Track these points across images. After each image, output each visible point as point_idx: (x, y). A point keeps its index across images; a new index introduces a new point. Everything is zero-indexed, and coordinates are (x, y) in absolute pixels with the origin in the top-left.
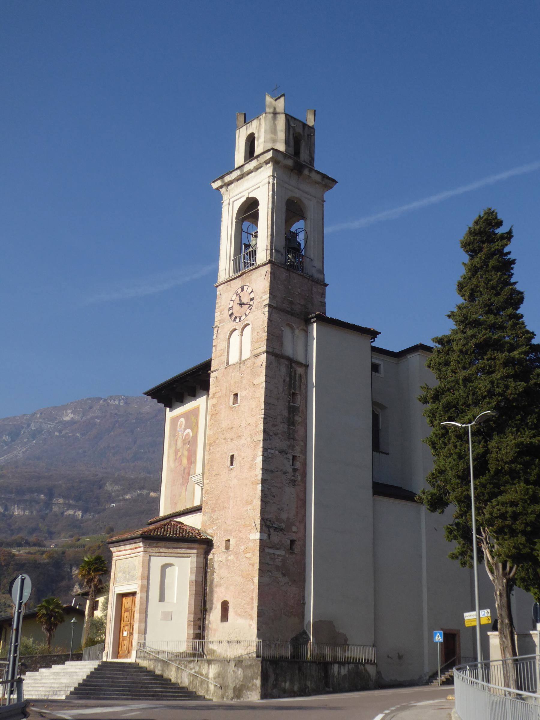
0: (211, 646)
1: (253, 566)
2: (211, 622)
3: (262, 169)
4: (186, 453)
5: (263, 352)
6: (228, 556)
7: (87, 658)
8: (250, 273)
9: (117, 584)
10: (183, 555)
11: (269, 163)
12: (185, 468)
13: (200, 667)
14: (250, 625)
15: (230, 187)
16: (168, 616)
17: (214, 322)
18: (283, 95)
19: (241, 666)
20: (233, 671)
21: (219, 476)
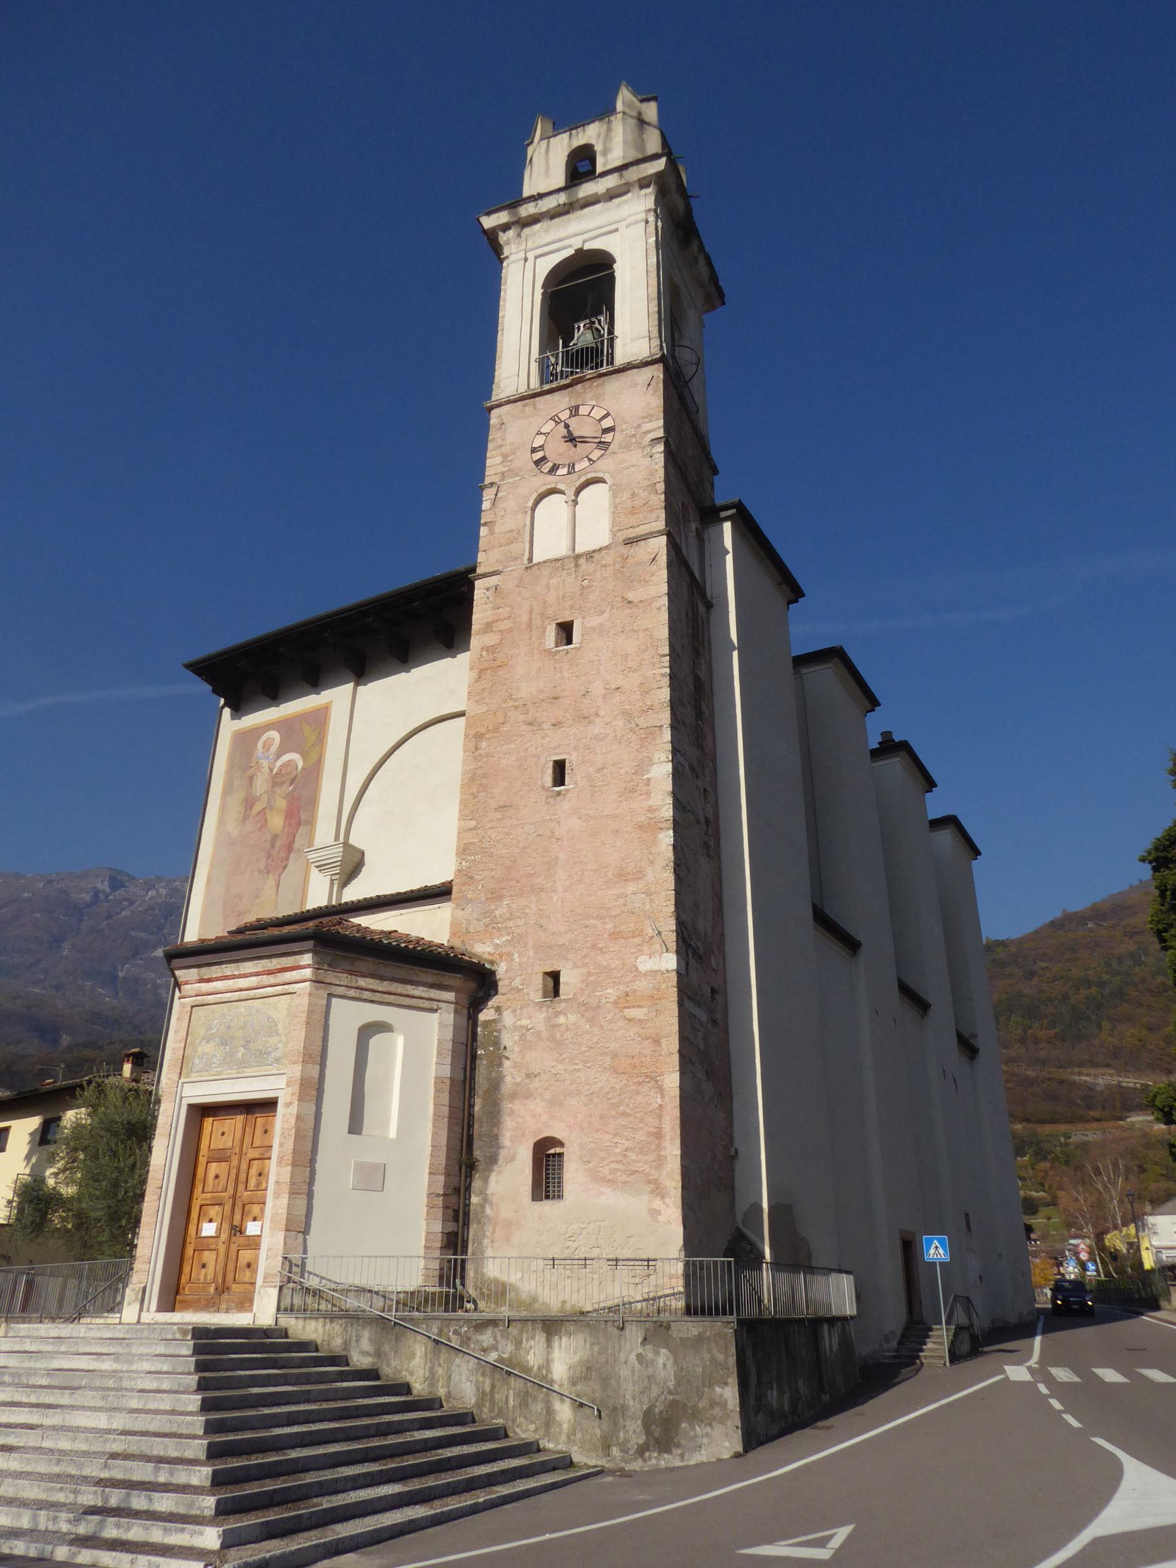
0: (492, 1270)
1: (657, 1042)
2: (495, 1199)
3: (624, 198)
4: (282, 804)
5: (660, 533)
6: (557, 1014)
7: (53, 1306)
8: (600, 381)
9: (194, 1077)
10: (421, 1003)
11: (648, 186)
12: (275, 837)
13: (518, 1344)
14: (654, 1213)
15: (527, 231)
16: (373, 1178)
17: (484, 476)
18: (655, 99)
19: (667, 1343)
20: (640, 1357)
21: (511, 812)
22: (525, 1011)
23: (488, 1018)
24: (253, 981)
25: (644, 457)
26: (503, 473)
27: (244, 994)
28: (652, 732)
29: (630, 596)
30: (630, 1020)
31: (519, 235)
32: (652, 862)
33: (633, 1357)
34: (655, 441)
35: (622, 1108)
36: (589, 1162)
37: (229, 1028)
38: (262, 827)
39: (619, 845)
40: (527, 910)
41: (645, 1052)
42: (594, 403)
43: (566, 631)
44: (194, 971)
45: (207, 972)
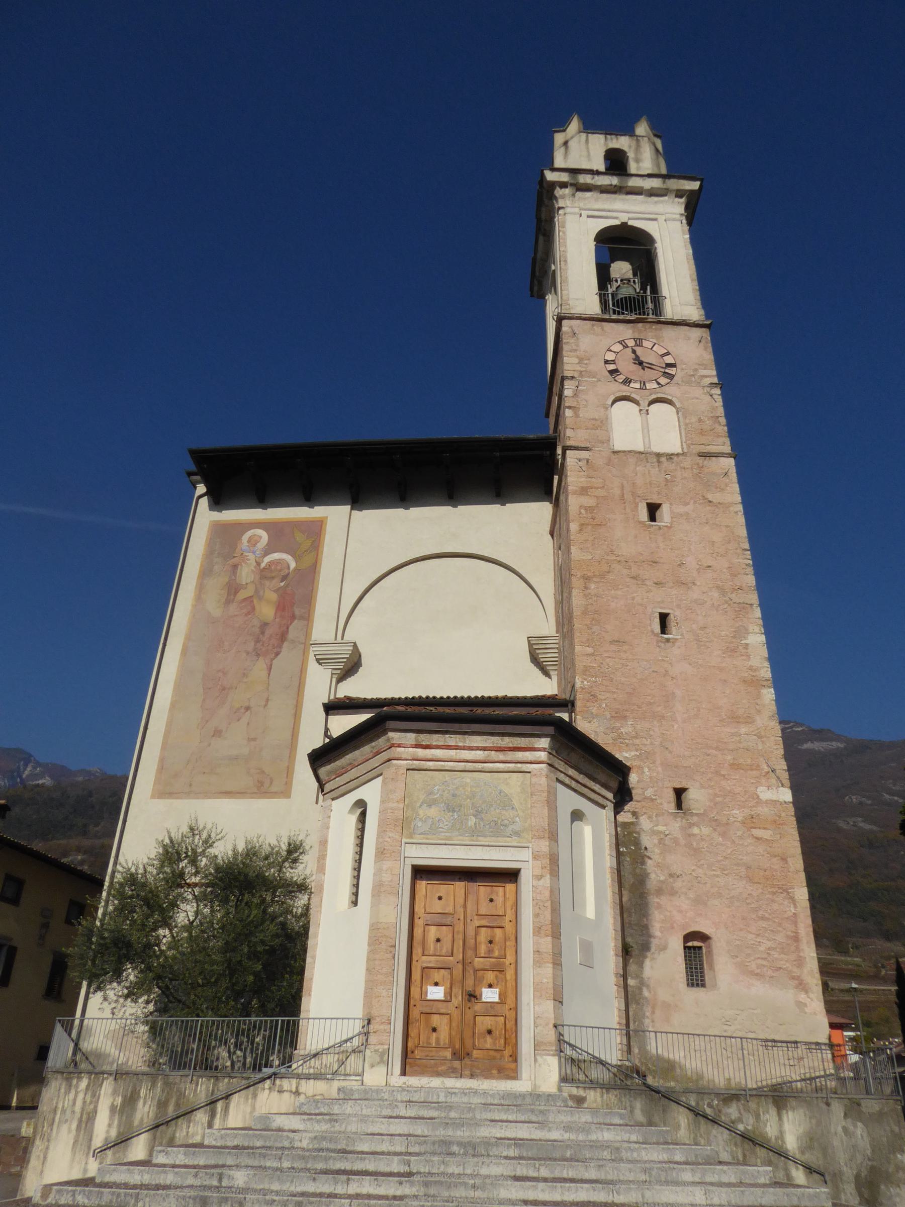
1: (784, 859)
6: (691, 825)
11: (680, 197)
13: (758, 1116)
14: (801, 1005)
20: (845, 1129)
21: (625, 647)
22: (660, 818)
23: (626, 820)
24: (480, 755)
25: (705, 394)
26: (581, 372)
27: (469, 766)
28: (744, 607)
29: (710, 497)
30: (758, 839)
31: (573, 195)
32: (759, 711)
33: (840, 1129)
34: (712, 385)
35: (760, 913)
36: (737, 957)
37: (454, 796)
38: (248, 613)
39: (728, 692)
40: (651, 733)
41: (775, 867)
42: (654, 341)
43: (653, 510)
44: (412, 736)
45: (425, 739)
